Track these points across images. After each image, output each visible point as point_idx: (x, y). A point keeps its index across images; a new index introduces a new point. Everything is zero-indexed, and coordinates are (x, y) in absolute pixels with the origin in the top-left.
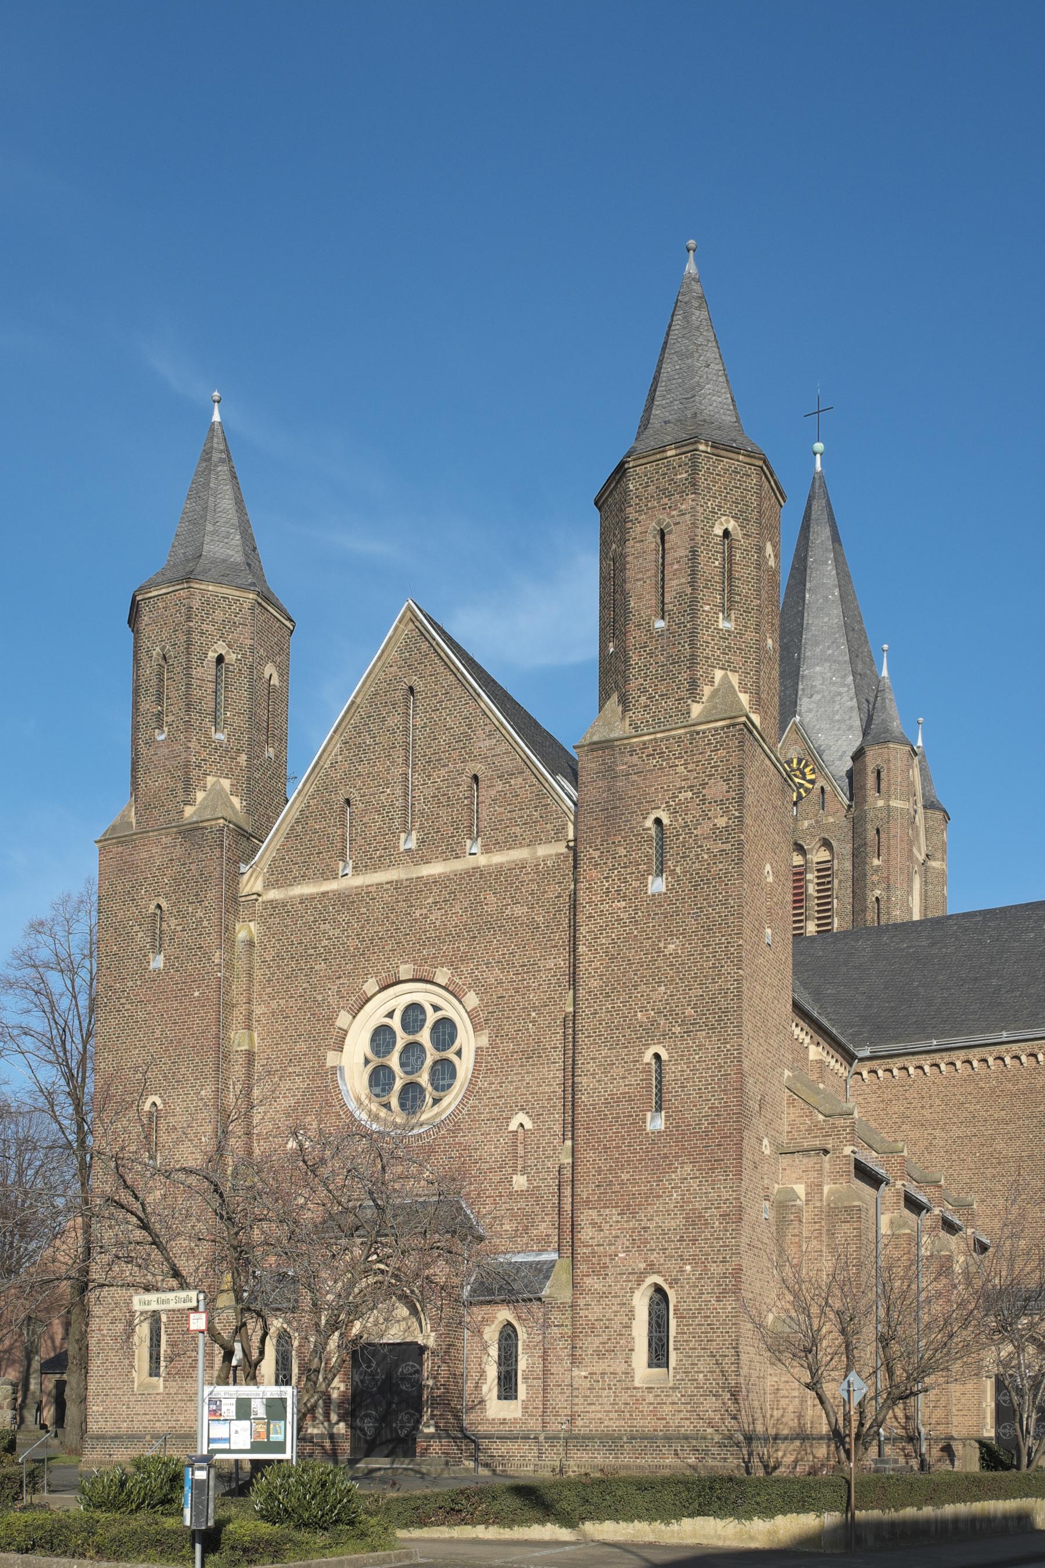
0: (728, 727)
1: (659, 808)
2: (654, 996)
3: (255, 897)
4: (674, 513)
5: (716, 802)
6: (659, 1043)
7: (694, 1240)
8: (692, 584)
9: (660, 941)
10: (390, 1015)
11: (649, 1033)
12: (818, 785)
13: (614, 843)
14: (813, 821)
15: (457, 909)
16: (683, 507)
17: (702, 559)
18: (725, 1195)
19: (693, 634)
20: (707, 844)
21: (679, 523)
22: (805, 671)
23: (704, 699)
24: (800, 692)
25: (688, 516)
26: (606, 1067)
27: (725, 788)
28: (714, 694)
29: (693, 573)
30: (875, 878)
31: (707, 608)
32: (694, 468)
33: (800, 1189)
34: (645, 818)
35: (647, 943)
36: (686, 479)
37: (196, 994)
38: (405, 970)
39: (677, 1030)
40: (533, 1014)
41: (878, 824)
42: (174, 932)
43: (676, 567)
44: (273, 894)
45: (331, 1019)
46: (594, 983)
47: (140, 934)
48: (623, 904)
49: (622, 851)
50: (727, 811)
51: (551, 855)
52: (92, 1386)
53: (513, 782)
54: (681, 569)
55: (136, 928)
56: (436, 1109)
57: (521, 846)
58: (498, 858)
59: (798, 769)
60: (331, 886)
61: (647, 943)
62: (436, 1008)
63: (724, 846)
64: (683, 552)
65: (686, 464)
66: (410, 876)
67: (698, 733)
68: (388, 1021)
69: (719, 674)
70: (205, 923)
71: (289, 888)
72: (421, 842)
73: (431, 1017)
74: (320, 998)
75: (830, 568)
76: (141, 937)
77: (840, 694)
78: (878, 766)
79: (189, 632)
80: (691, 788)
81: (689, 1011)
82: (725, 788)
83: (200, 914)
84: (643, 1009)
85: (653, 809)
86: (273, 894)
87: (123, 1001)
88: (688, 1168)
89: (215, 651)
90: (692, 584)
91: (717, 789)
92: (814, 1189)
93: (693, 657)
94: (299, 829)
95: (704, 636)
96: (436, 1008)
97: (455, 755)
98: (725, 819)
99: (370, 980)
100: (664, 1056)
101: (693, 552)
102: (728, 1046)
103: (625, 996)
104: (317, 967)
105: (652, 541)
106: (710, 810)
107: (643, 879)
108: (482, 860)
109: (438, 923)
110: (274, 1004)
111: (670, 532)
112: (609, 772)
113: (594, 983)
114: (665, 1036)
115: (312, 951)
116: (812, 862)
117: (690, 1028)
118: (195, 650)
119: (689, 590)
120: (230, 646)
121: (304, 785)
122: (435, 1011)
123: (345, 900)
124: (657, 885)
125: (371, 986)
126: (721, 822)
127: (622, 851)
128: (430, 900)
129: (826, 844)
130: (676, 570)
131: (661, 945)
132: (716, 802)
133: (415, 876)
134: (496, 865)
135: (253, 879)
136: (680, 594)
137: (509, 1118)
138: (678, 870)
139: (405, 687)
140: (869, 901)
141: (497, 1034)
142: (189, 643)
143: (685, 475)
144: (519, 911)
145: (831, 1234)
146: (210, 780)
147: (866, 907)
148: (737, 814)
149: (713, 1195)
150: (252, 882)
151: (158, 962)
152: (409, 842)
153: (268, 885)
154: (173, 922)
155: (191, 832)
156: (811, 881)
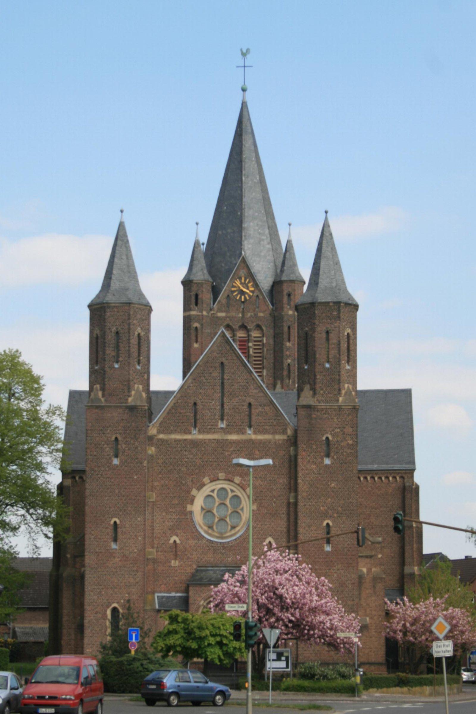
2: (327, 502)
7: (342, 592)
8: (339, 353)
11: (326, 515)
12: (255, 294)
14: (253, 314)
17: (342, 345)
18: (353, 576)
19: (339, 372)
20: (346, 449)
22: (245, 225)
23: (343, 395)
24: (243, 238)
26: (309, 526)
28: (346, 393)
29: (339, 350)
30: (288, 353)
32: (339, 311)
33: (365, 570)
35: (324, 482)
37: (135, 477)
39: (335, 515)
40: (275, 500)
41: (289, 324)
42: (124, 450)
43: (333, 346)
44: (161, 436)
45: (189, 492)
46: (305, 494)
47: (108, 449)
49: (314, 447)
50: (352, 439)
52: (86, 641)
55: (106, 446)
56: (233, 532)
57: (269, 433)
58: (260, 437)
60: (188, 437)
61: (324, 482)
62: (232, 491)
64: (335, 341)
68: (211, 494)
69: (346, 385)
70: (139, 448)
72: (228, 425)
73: (230, 495)
74: (184, 482)
75: (254, 163)
76: (108, 450)
77: (263, 240)
79: (129, 324)
80: (339, 428)
81: (340, 509)
82: (351, 430)
83: (137, 444)
84: (323, 506)
86: (161, 436)
87: (99, 476)
88: (340, 566)
91: (349, 430)
92: (369, 570)
93: (339, 380)
94: (173, 411)
95: (343, 372)
96: (232, 491)
97: (242, 393)
100: (331, 524)
101: (339, 342)
104: (182, 469)
105: (324, 335)
107: (322, 458)
108: (253, 437)
110: (162, 482)
112: (309, 416)
113: (305, 494)
114: (331, 517)
115: (180, 463)
116: (251, 336)
118: (131, 332)
119: (338, 356)
120: (142, 329)
123: (195, 444)
124: (327, 461)
126: (350, 442)
127: (314, 447)
128: (232, 449)
129: (259, 327)
131: (329, 483)
138: (335, 457)
139: (220, 362)
140: (284, 365)
141: (260, 506)
142: (129, 329)
145: (374, 587)
146: (136, 386)
147: (283, 368)
149: (349, 576)
150: (153, 431)
151: (116, 461)
153: (159, 432)
154: (124, 446)
155: (132, 409)
156: (251, 347)
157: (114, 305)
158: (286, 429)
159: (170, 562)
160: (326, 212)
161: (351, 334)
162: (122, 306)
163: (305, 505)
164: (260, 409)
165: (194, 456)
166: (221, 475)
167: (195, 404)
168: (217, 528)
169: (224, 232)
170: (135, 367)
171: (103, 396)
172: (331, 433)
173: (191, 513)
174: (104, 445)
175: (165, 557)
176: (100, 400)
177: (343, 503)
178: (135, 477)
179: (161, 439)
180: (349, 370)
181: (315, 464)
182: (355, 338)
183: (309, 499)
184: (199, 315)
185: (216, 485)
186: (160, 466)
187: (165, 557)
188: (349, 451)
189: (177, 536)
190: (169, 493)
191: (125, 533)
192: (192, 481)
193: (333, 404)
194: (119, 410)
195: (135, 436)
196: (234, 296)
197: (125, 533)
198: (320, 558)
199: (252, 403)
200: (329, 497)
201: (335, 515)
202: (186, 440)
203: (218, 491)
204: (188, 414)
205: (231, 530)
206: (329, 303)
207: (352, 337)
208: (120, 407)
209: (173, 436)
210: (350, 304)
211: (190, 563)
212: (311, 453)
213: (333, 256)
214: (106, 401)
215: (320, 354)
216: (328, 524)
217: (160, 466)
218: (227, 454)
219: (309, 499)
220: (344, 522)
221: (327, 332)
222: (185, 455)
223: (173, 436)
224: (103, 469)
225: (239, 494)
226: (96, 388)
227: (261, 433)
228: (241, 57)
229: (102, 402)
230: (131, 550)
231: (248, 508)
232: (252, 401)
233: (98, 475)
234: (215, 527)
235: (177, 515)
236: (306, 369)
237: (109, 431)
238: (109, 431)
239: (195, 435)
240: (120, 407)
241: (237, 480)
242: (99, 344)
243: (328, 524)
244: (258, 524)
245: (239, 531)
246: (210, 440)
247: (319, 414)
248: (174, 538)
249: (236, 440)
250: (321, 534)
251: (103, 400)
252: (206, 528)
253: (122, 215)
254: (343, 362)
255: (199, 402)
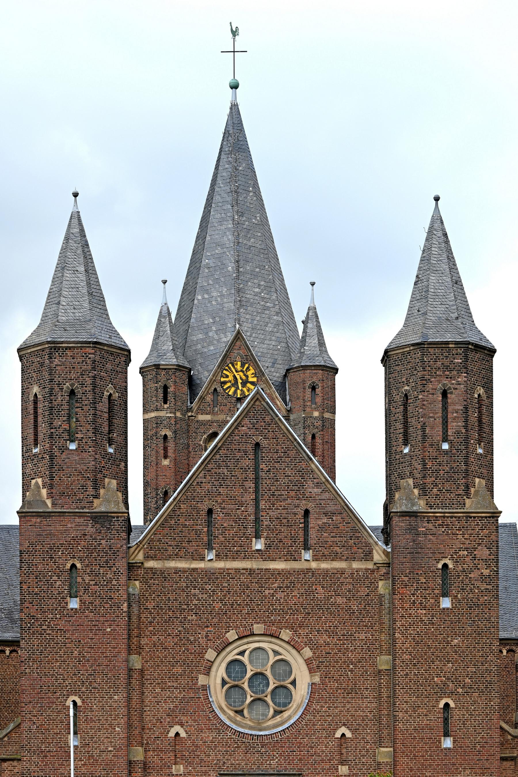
0: (489, 517)
1: (447, 557)
3: (140, 565)
4: (453, 382)
5: (482, 560)
6: (449, 697)
9: (448, 637)
10: (242, 653)
11: (443, 692)
13: (417, 574)
15: (295, 593)
16: (459, 380)
20: (479, 584)
21: (456, 389)
25: (462, 386)
27: (488, 552)
31: (472, 442)
34: (438, 562)
36: (461, 363)
37: (109, 630)
38: (258, 628)
39: (460, 690)
42: (89, 585)
44: (151, 564)
45: (201, 654)
47: (58, 583)
48: (424, 612)
50: (488, 567)
51: (362, 569)
53: (334, 518)
54: (458, 417)
56: (278, 719)
57: (341, 559)
59: (242, 371)
60: (201, 565)
63: (488, 587)
65: (461, 354)
66: (260, 567)
67: (471, 517)
71: (166, 561)
72: (268, 546)
78: (313, 383)
80: (467, 549)
81: (467, 680)
82: (488, 552)
84: (438, 676)
85: (443, 557)
86: (151, 564)
87: (44, 627)
89: (108, 391)
90: (466, 427)
91: (483, 552)
97: (293, 494)
98: (488, 571)
99: (231, 631)
100: (452, 705)
102: (492, 703)
103: (425, 667)
104: (189, 618)
106: (479, 564)
108: (314, 565)
109: (282, 601)
110: (155, 638)
111: (451, 393)
112: (413, 530)
117: (468, 690)
119: (464, 431)
121: (178, 494)
122: (275, 656)
123: (210, 575)
124: (446, 603)
125: (232, 635)
126: (486, 572)
128: (276, 585)
130: (455, 417)
131: (449, 639)
132: (482, 560)
133: (264, 567)
134: (323, 569)
135: (137, 551)
136: (458, 432)
137: (335, 730)
141: (324, 677)
143: (460, 361)
144: (339, 600)
148: (495, 569)
151: (74, 604)
152: (259, 545)
154: (87, 578)
157: (66, 345)
158: (371, 552)
159: (170, 768)
160: (437, 199)
161: (484, 396)
162: (81, 347)
163: (407, 674)
164: (325, 521)
165: (210, 597)
166: (258, 628)
167: (210, 512)
168: (249, 713)
169: (206, 296)
170: (105, 451)
171: (50, 495)
172: (452, 558)
173: (205, 688)
174: (51, 576)
175: (162, 759)
176: (45, 503)
177: (474, 670)
178: (109, 630)
179: (151, 569)
180: (481, 455)
181: (425, 608)
182: (491, 405)
183: (415, 665)
184: (169, 418)
185: (248, 643)
186: (151, 613)
187: (162, 759)
188: (484, 586)
189: (182, 725)
190: (166, 657)
191: (92, 720)
192: (207, 636)
193: (455, 511)
194: (77, 520)
195: (107, 562)
196: (224, 390)
197: (92, 720)
198: (434, 760)
199: (310, 509)
200: (448, 662)
201: (460, 690)
202: (194, 570)
203: (251, 652)
204: (198, 527)
205: (273, 717)
206: (447, 343)
207: (486, 402)
208: (80, 515)
209: (172, 564)
210: (484, 348)
211: (204, 769)
212: (417, 589)
213: (450, 269)
214: (53, 504)
215: (432, 428)
216: (447, 705)
217: (151, 613)
218: (267, 592)
219: (415, 665)
220: (475, 702)
221: (445, 394)
222: (195, 595)
223: (172, 564)
224: (50, 616)
225: (289, 658)
226: (37, 483)
227: (326, 560)
228: (231, 35)
229: (48, 507)
230: (102, 747)
231: (303, 679)
232: (310, 506)
233: (41, 625)
234: (246, 712)
235: (180, 692)
236: (406, 454)
237: (60, 553)
238: (60, 553)
239: (211, 561)
240: (80, 515)
241: (286, 634)
242: (40, 411)
243: (447, 705)
244: (322, 707)
245: (290, 718)
246: (237, 570)
247: (430, 526)
248: (177, 728)
249: (283, 570)
250: (436, 719)
251: (49, 502)
252: (232, 714)
253: (76, 201)
254: (472, 442)
255: (217, 509)
